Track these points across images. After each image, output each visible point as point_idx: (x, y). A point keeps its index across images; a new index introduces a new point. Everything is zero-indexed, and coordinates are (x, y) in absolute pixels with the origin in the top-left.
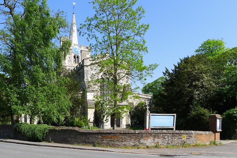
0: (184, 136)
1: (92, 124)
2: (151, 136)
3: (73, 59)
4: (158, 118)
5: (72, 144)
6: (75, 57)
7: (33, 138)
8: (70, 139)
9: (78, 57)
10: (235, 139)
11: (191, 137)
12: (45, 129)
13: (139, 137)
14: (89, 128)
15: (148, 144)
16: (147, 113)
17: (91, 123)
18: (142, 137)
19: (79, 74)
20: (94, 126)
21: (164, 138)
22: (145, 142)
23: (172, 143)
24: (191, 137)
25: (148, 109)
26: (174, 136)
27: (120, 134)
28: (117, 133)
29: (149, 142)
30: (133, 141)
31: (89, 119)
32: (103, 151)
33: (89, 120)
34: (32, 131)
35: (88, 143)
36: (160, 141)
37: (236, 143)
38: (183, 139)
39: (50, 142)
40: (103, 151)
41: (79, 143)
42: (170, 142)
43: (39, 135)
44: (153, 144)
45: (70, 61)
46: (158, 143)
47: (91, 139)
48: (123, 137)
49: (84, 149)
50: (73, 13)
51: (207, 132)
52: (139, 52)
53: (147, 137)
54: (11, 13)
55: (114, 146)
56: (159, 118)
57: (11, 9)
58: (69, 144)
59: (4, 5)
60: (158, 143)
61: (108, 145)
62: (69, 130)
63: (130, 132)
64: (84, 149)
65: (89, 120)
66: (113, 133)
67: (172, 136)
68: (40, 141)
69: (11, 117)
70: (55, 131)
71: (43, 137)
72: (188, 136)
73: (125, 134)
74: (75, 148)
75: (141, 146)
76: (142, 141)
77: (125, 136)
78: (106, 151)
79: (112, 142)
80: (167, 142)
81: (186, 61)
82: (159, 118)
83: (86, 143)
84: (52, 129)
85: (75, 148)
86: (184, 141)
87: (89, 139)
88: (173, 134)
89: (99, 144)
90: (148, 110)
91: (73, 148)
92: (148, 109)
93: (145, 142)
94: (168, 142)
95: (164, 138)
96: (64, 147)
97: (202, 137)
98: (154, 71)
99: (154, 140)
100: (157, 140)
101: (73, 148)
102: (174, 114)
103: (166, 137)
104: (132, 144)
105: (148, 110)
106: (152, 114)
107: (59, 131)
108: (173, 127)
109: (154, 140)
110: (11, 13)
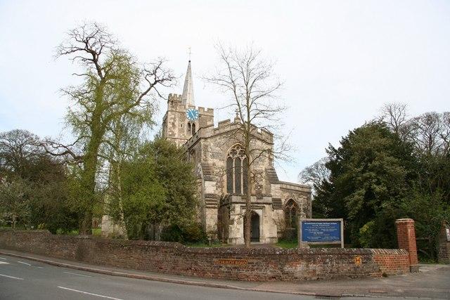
2: (302, 259)
3: (186, 127)
6: (189, 124)
9: (194, 125)
10: (447, 263)
11: (369, 259)
18: (287, 261)
19: (194, 151)
21: (325, 263)
37: (447, 269)
45: (181, 131)
48: (255, 261)
52: (235, 223)
53: (296, 260)
54: (95, 61)
57: (94, 55)
67: (338, 258)
77: (259, 259)
81: (357, 131)
94: (331, 270)
95: (325, 263)
98: (142, 58)
99: (307, 266)
100: (312, 266)
102: (340, 220)
109: (307, 266)
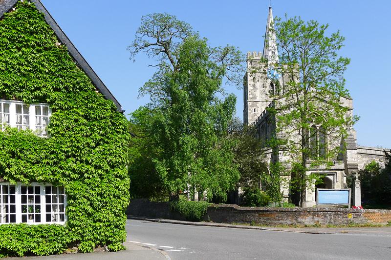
0: (350, 214)
1: (287, 199)
2: (310, 214)
4: (333, 194)
5: (230, 223)
7: (191, 217)
8: (228, 218)
12: (204, 206)
13: (296, 214)
14: (280, 206)
15: (306, 223)
16: (356, 183)
17: (284, 197)
20: (289, 202)
22: (303, 220)
23: (335, 222)
24: (360, 216)
25: (357, 177)
26: (337, 214)
27: (277, 211)
28: (273, 211)
29: (308, 220)
30: (290, 220)
31: (281, 192)
32: (256, 229)
33: (283, 193)
34: (190, 209)
35: (246, 221)
36: (320, 220)
38: (349, 218)
39: (208, 222)
40: (256, 229)
41: (237, 222)
42: (332, 221)
43: (197, 213)
44: (312, 223)
46: (318, 221)
47: (249, 217)
48: (280, 215)
49: (239, 228)
50: (270, 8)
51: (384, 211)
53: (305, 215)
55: (270, 225)
56: (329, 194)
58: (228, 223)
59: (157, 44)
60: (318, 221)
61: (266, 224)
62: (227, 208)
63: (286, 210)
64: (239, 228)
65: (283, 193)
66: (270, 211)
68: (198, 221)
69: (179, 143)
70: (213, 208)
71: (202, 215)
72: (355, 215)
73: (282, 211)
74: (230, 227)
75: (298, 225)
76: (299, 219)
78: (258, 229)
79: (269, 221)
80: (328, 221)
82: (329, 194)
83: (244, 221)
84: (211, 206)
85: (230, 227)
86: (350, 220)
87: (246, 217)
88: (335, 212)
89: (257, 223)
90: (357, 180)
91: (228, 227)
92: (357, 177)
93: (303, 220)
96: (220, 226)
97: (374, 216)
99: (313, 218)
100: (316, 219)
101: (228, 227)
103: (327, 215)
104: (289, 222)
105: (357, 180)
106: (319, 189)
107: (218, 209)
108: (347, 205)
109: (313, 218)
110: (165, 51)
